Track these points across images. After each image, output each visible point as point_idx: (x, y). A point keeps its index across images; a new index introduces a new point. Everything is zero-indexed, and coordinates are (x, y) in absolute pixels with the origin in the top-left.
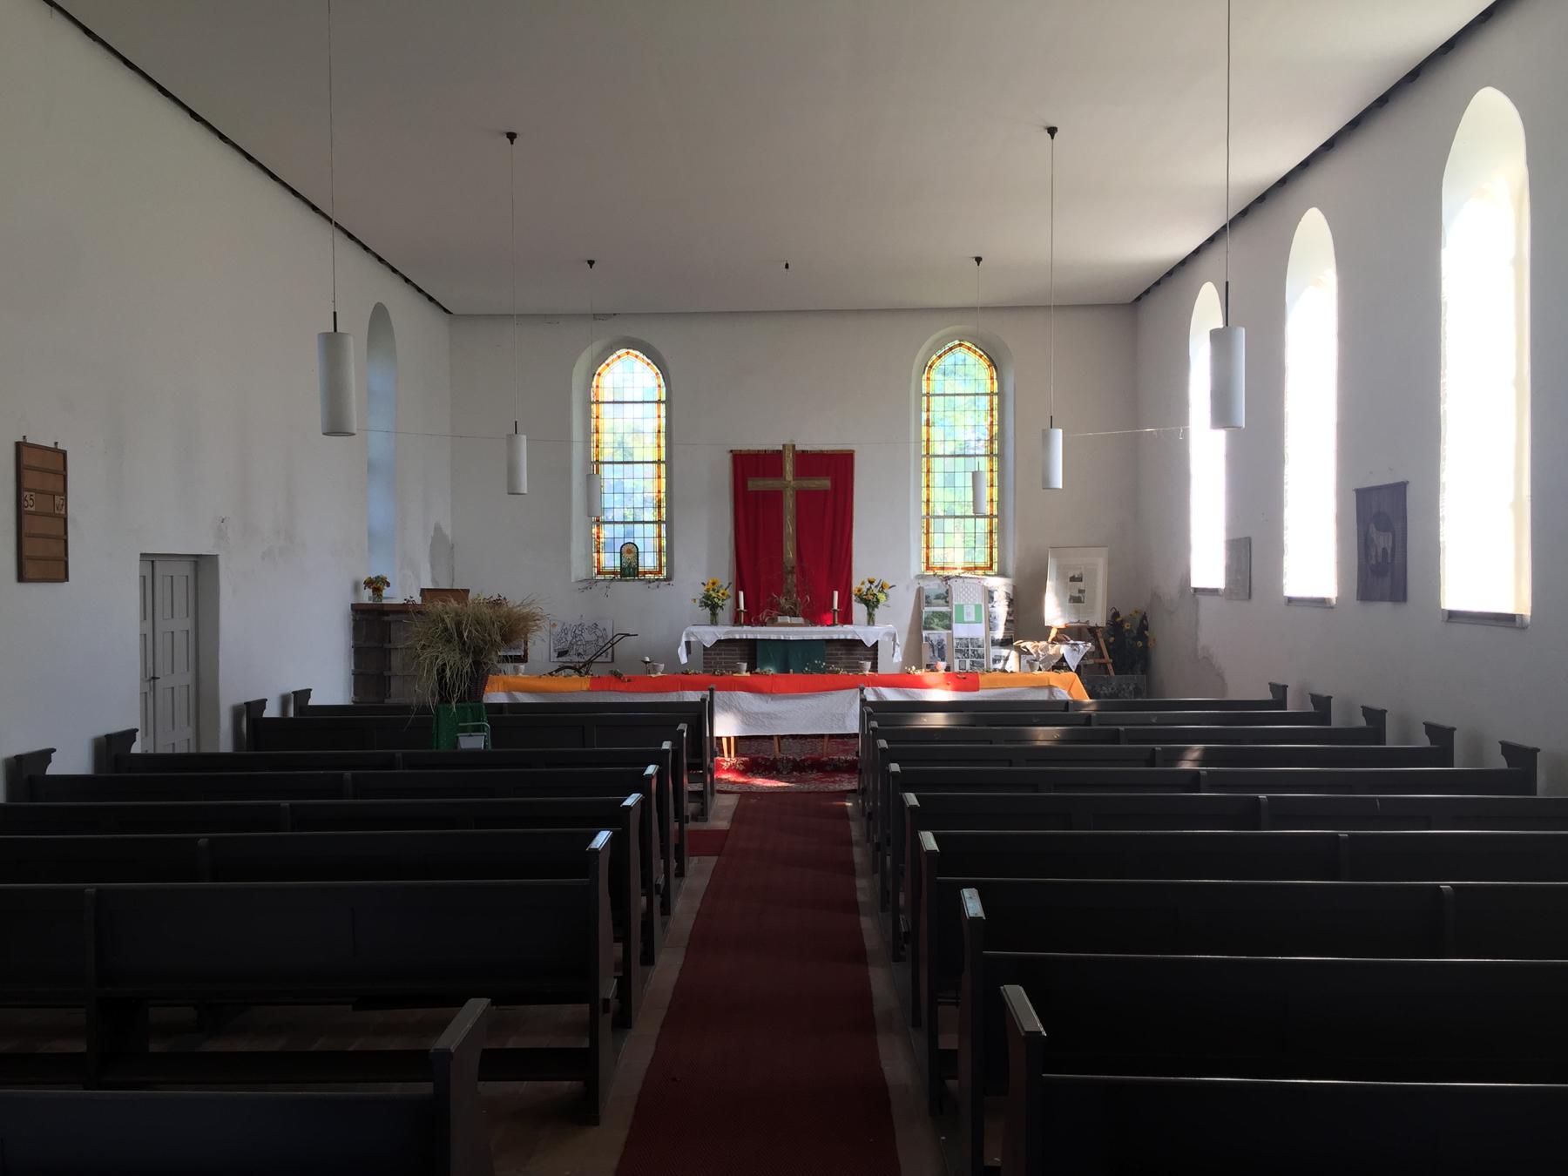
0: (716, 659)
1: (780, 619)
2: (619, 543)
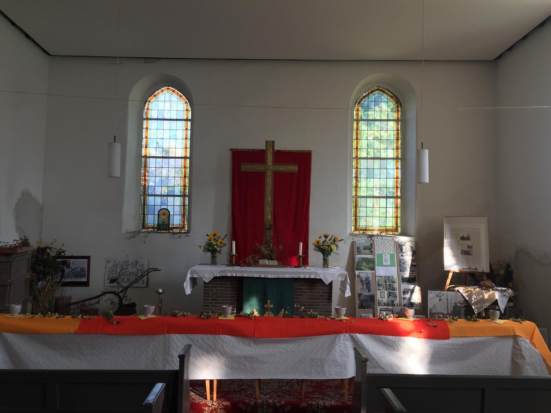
0: (213, 290)
1: (261, 262)
2: (157, 209)
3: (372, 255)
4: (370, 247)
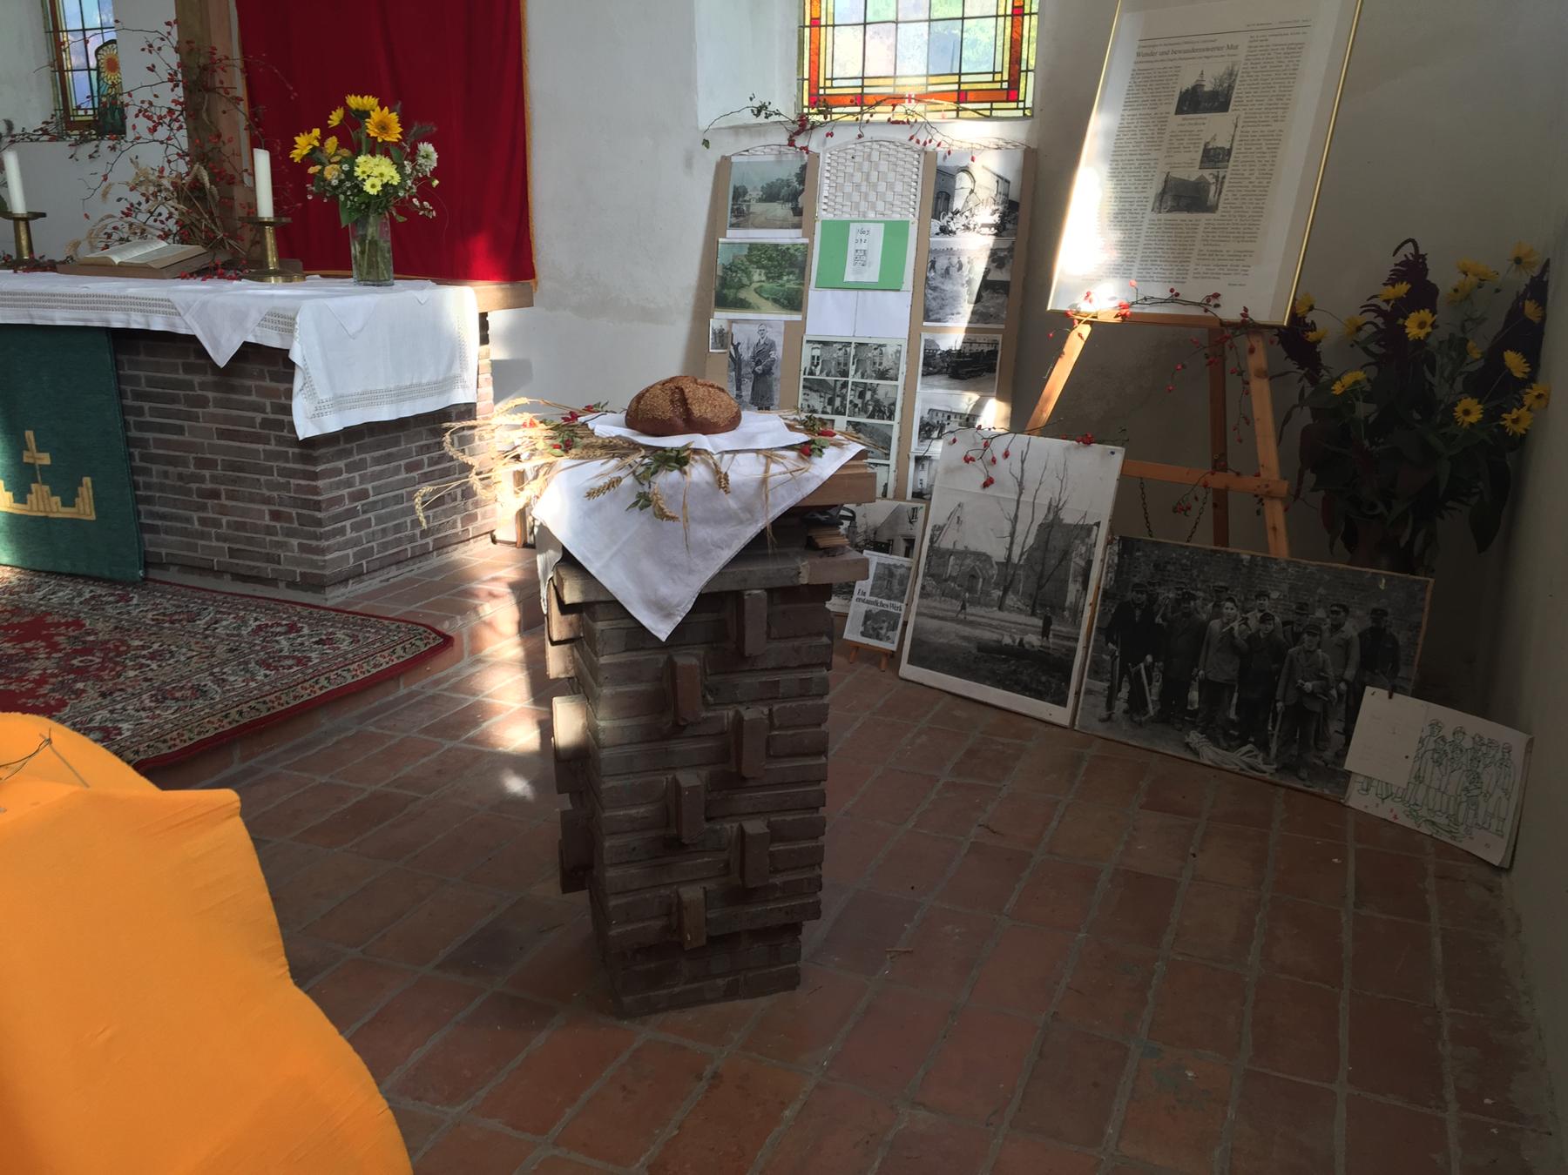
3: (798, 232)
4: (796, 184)
